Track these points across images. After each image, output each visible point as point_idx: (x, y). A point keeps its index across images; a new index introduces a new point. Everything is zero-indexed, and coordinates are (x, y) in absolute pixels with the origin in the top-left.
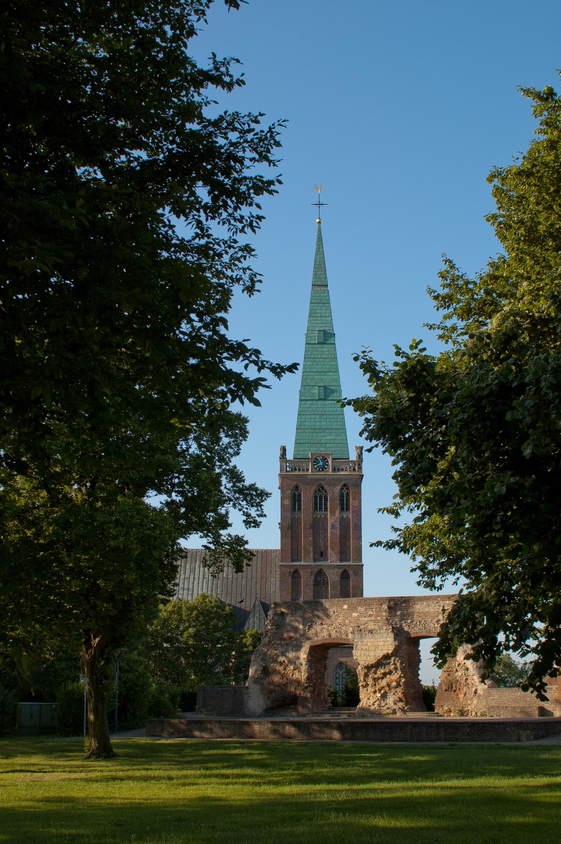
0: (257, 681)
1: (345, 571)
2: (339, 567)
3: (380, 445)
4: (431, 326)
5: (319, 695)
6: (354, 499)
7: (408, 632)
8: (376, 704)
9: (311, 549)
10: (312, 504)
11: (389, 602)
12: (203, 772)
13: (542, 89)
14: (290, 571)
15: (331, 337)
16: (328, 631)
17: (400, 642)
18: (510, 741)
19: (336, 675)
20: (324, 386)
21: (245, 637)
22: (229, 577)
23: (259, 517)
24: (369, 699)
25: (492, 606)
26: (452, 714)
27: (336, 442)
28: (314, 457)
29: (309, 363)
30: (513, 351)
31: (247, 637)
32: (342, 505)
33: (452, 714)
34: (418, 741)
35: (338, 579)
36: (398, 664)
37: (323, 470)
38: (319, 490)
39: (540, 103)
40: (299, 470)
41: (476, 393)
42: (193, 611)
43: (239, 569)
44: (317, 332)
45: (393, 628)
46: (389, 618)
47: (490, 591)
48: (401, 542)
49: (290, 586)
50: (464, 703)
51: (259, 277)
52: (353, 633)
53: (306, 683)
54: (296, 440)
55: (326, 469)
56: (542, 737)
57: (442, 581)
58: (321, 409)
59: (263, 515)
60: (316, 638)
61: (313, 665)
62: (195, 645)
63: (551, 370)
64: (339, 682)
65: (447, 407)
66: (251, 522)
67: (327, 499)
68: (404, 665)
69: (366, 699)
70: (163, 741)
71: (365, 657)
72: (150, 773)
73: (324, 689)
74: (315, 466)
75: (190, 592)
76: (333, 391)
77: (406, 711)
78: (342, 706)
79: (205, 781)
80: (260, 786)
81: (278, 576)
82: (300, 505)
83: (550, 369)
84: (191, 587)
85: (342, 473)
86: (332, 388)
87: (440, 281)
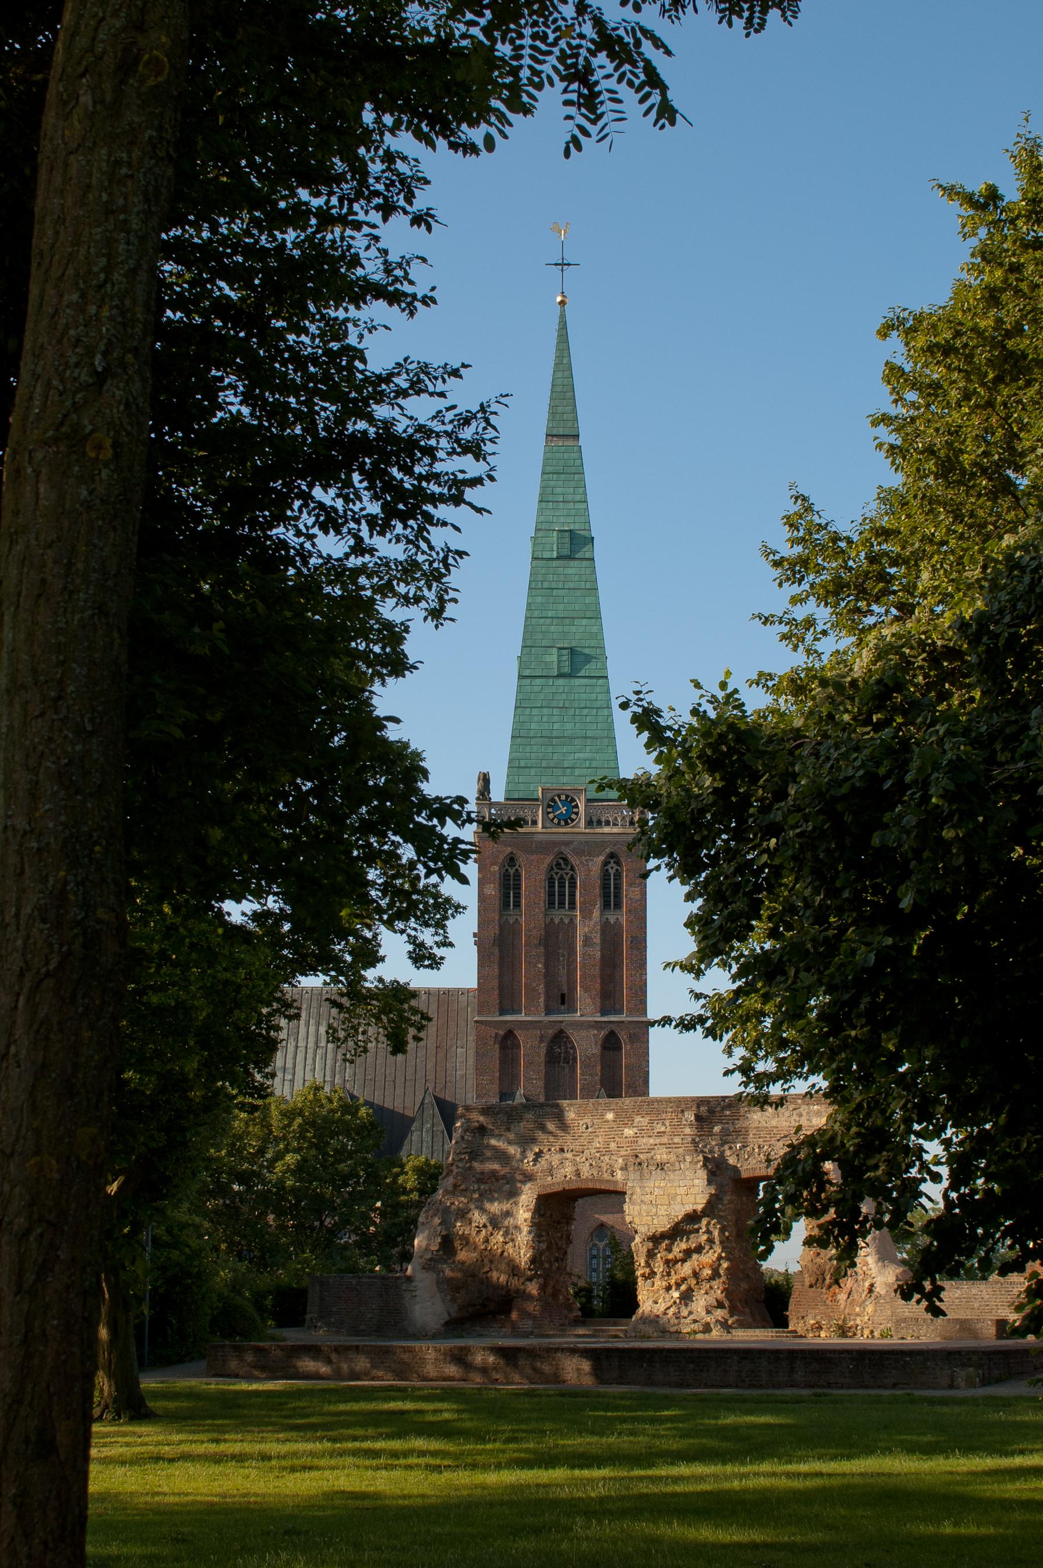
0: (431, 1265)
1: (612, 1033)
2: (598, 1025)
3: (663, 866)
4: (767, 619)
5: (555, 1294)
6: (630, 884)
7: (735, 1167)
8: (671, 1312)
9: (541, 988)
10: (543, 895)
11: (698, 1107)
12: (328, 1445)
13: (977, 187)
14: (497, 1034)
15: (585, 545)
16: (575, 1164)
17: (720, 1188)
18: (934, 1388)
19: (591, 1249)
20: (571, 648)
21: (403, 1173)
23: (439, 947)
24: (656, 1302)
25: (850, 1156)
26: (823, 1334)
27: (594, 764)
28: (549, 796)
29: (539, 599)
30: (896, 709)
31: (406, 1173)
32: (606, 896)
33: (823, 1334)
34: (752, 1386)
35: (596, 1050)
36: (716, 1233)
37: (567, 823)
38: (558, 864)
39: (972, 212)
41: (827, 792)
42: (294, 1119)
43: (398, 1046)
44: (555, 534)
45: (706, 1159)
46: (697, 1139)
47: (848, 1129)
48: (708, 1018)
50: (847, 1311)
51: (452, 594)
52: (625, 1168)
53: (529, 1269)
54: (511, 761)
55: (573, 820)
56: (999, 1381)
57: (784, 1090)
58: (564, 696)
59: (446, 944)
60: (549, 1178)
61: (544, 1233)
62: (299, 1189)
63: (947, 765)
64: (598, 1264)
65: (778, 809)
66: (421, 956)
67: (575, 883)
68: (727, 1234)
69: (650, 1302)
70: (244, 1386)
71: (649, 1218)
72: (223, 1447)
73: (565, 1282)
74: (551, 816)
75: (289, 1077)
76: (588, 659)
77: (730, 1327)
78: (602, 1316)
79: (333, 1462)
80: (441, 1472)
81: (472, 1045)
82: (518, 896)
83: (945, 763)
84: (289, 1065)
85: (606, 830)
86: (587, 651)
87: (786, 532)
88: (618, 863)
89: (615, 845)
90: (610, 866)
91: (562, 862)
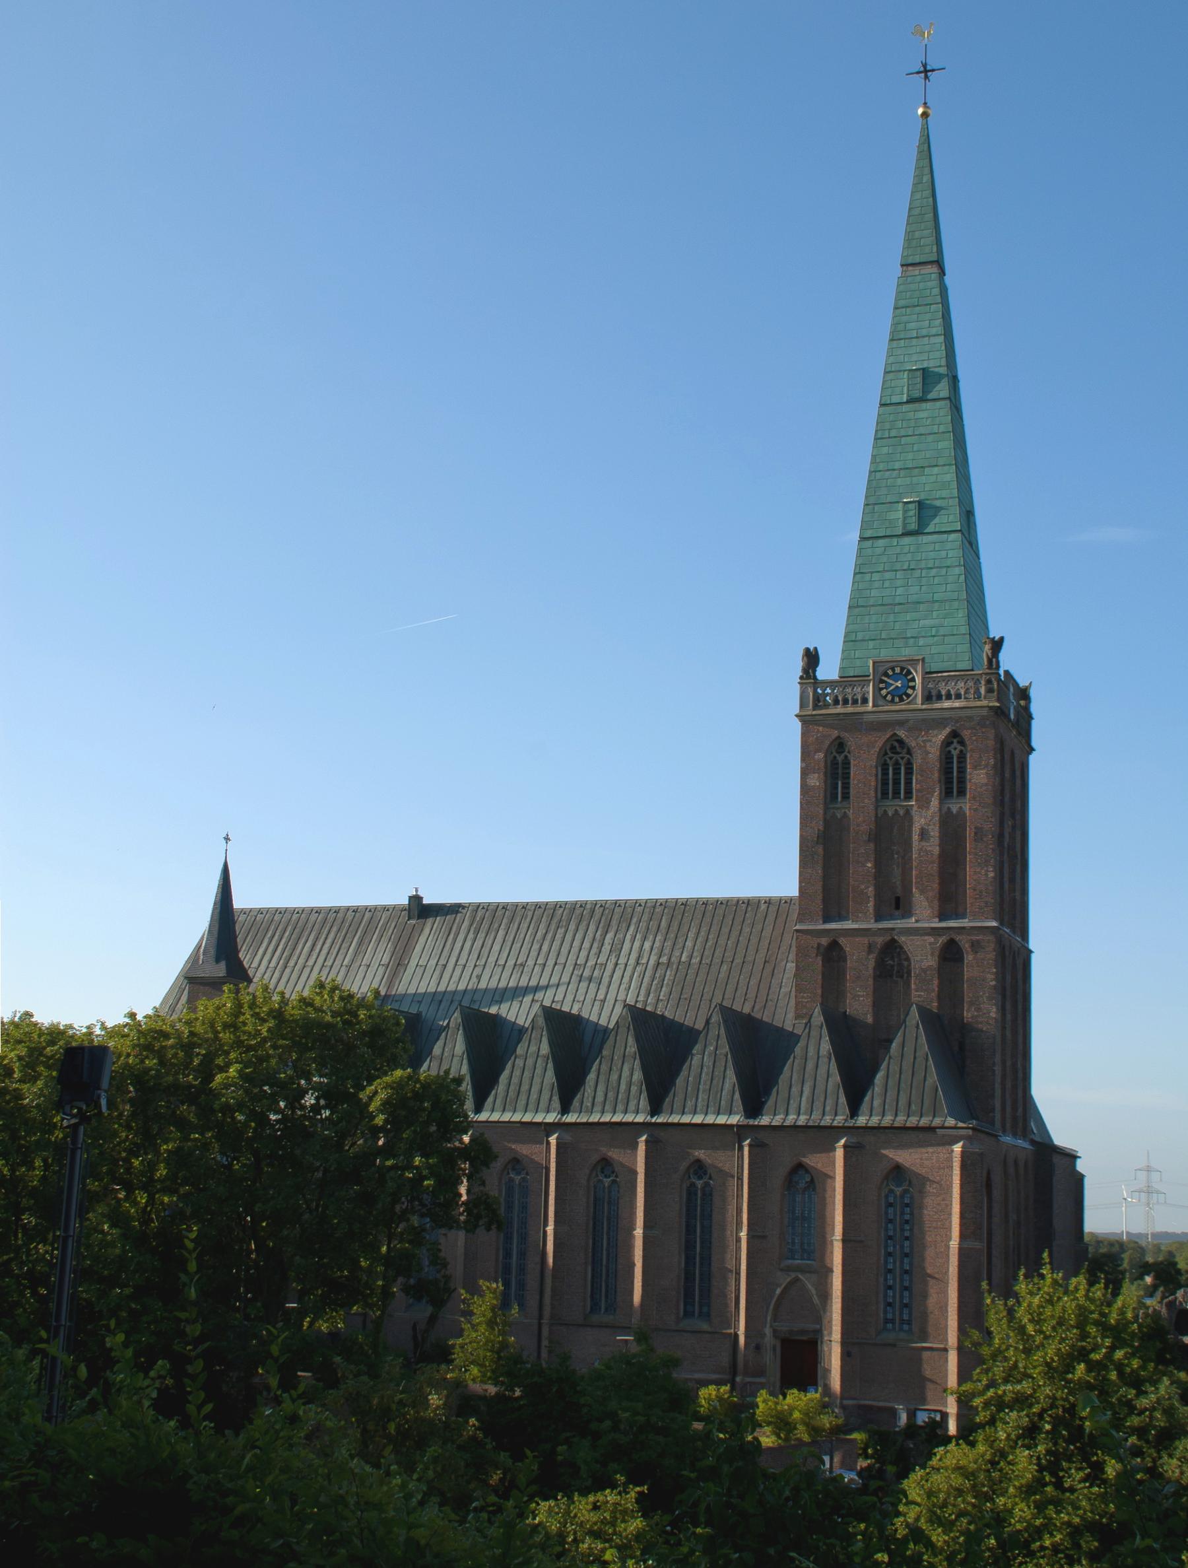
1: (952, 942)
2: (935, 932)
14: (819, 945)
27: (942, 631)
28: (881, 669)
29: (885, 450)
35: (931, 962)
37: (901, 700)
38: (893, 748)
49: (820, 981)
58: (909, 557)
74: (884, 692)
82: (846, 786)
85: (947, 704)
86: (938, 503)
88: (962, 743)
89: (957, 722)
90: (953, 746)
91: (897, 746)
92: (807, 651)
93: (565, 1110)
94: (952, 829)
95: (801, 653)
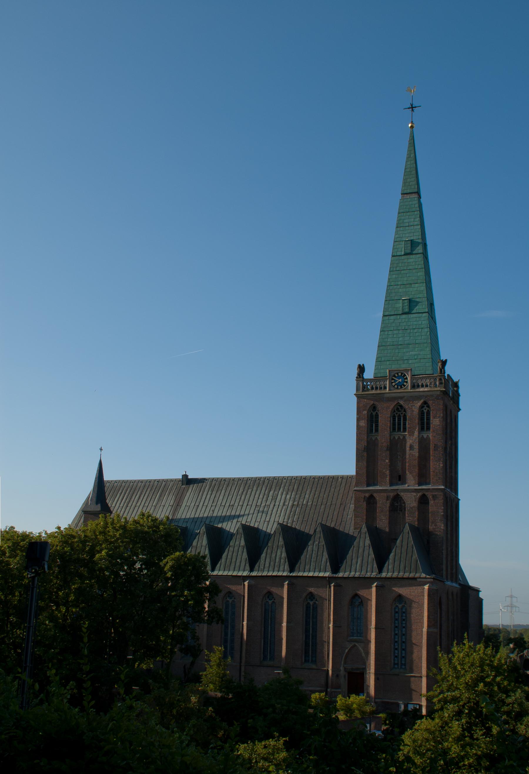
2: (416, 491)
14: (365, 497)
22: (309, 504)
27: (419, 357)
28: (392, 374)
29: (394, 276)
35: (415, 504)
37: (401, 387)
40: (377, 388)
44: (403, 242)
58: (405, 324)
74: (394, 384)
82: (377, 426)
85: (422, 389)
86: (418, 300)
88: (428, 406)
89: (426, 397)
90: (424, 408)
91: (399, 408)
92: (359, 366)
93: (252, 570)
94: (424, 445)
95: (357, 367)
